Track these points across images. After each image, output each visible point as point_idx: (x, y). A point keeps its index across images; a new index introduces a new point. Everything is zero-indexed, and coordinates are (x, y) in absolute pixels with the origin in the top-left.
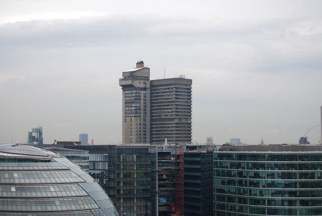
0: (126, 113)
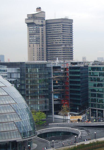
0: (30, 41)
